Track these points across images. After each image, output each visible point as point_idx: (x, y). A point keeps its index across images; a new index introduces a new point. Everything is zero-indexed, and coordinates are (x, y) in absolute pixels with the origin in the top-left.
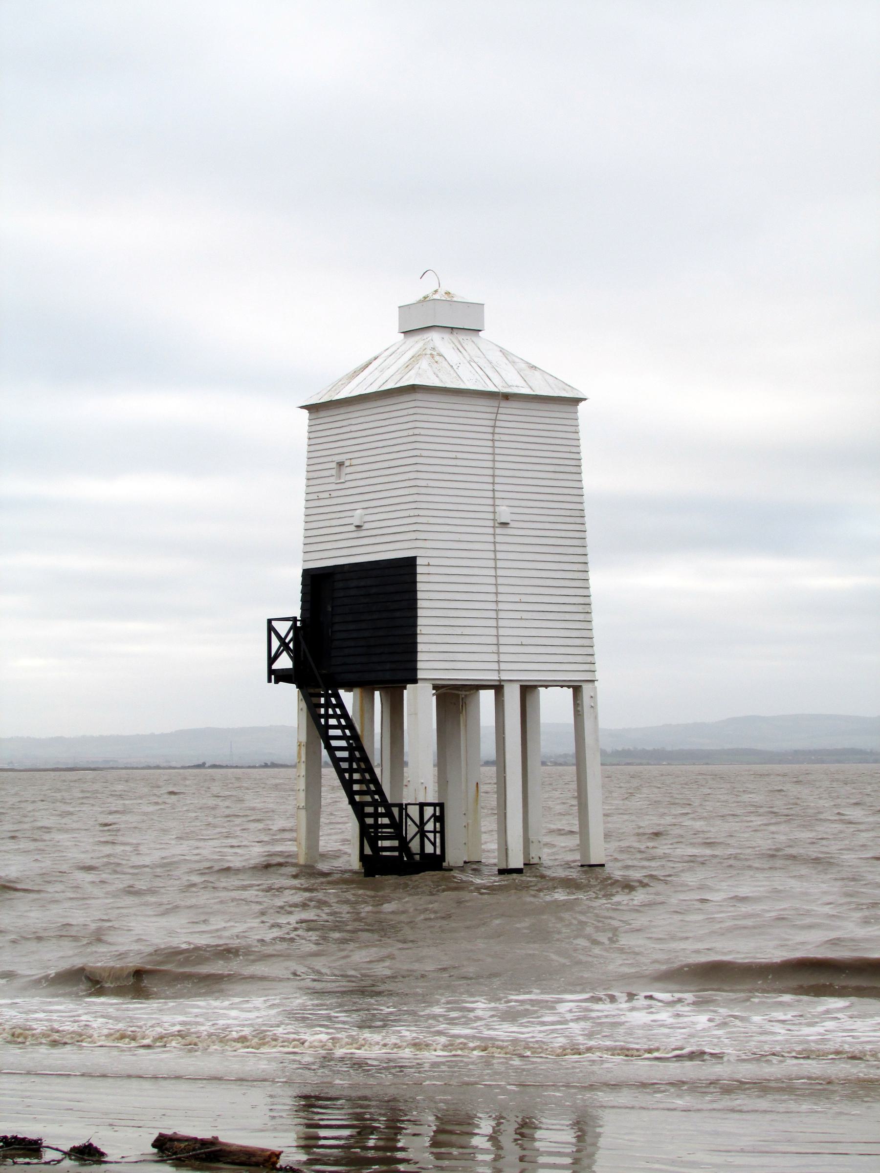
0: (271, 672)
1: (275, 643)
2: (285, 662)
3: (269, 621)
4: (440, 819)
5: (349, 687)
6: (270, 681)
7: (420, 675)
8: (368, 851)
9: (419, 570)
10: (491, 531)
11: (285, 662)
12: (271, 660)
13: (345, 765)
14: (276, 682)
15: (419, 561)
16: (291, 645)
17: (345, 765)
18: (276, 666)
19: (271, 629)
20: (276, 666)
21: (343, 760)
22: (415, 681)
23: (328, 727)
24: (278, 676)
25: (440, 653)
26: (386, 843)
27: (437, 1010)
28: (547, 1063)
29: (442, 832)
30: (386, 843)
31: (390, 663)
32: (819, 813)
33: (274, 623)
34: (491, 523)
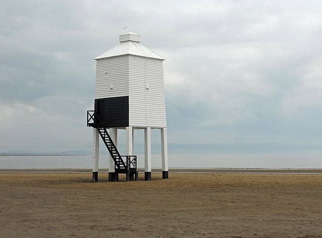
0: (88, 124)
2: (92, 121)
3: (88, 111)
4: (135, 160)
5: (109, 127)
7: (130, 125)
8: (117, 167)
11: (92, 121)
12: (88, 121)
13: (114, 149)
16: (93, 117)
17: (114, 149)
19: (88, 113)
21: (114, 151)
22: (128, 126)
23: (112, 150)
24: (90, 125)
25: (134, 118)
26: (102, 131)
29: (136, 163)
30: (102, 131)
31: (123, 122)
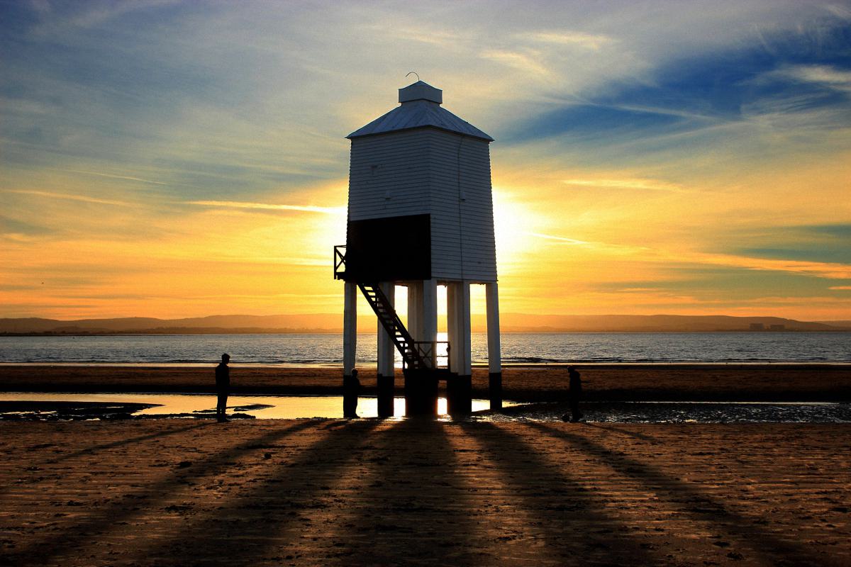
0: (336, 273)
1: (339, 260)
2: (342, 269)
3: (335, 247)
6: (335, 278)
7: (433, 275)
9: (432, 221)
10: (458, 203)
11: (342, 269)
12: (336, 268)
14: (339, 279)
15: (431, 216)
18: (338, 271)
19: (336, 251)
20: (338, 271)
24: (338, 276)
27: (351, 460)
28: (723, 488)
32: (96, 430)
33: (338, 248)
34: (458, 199)
